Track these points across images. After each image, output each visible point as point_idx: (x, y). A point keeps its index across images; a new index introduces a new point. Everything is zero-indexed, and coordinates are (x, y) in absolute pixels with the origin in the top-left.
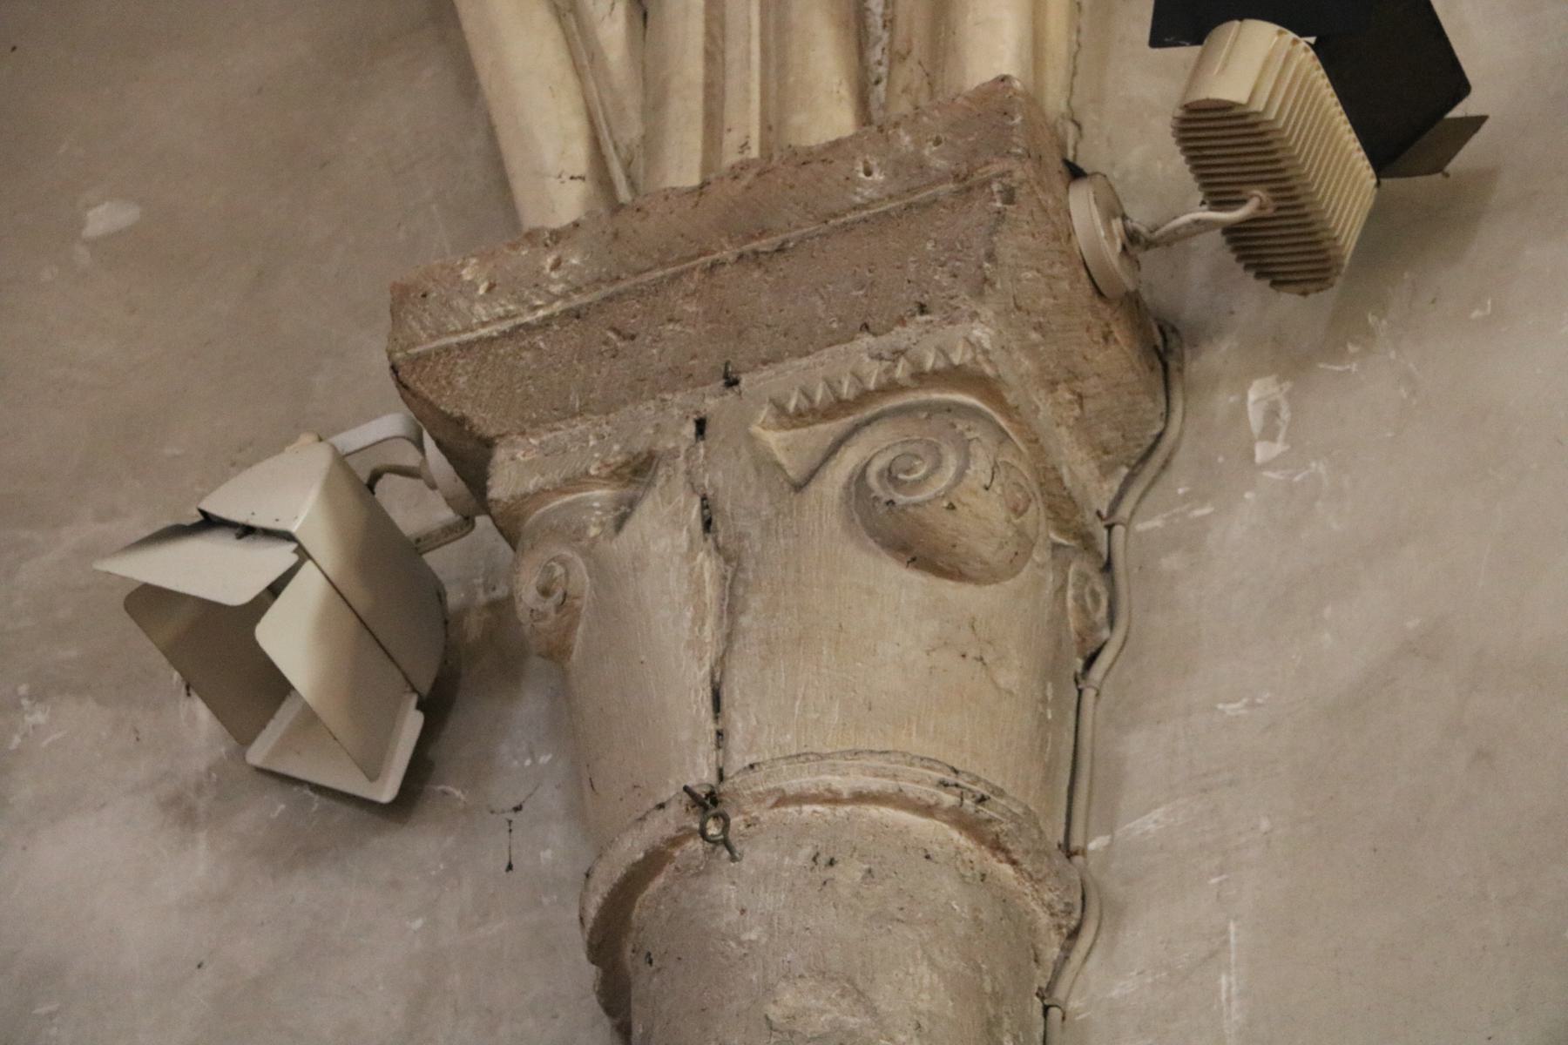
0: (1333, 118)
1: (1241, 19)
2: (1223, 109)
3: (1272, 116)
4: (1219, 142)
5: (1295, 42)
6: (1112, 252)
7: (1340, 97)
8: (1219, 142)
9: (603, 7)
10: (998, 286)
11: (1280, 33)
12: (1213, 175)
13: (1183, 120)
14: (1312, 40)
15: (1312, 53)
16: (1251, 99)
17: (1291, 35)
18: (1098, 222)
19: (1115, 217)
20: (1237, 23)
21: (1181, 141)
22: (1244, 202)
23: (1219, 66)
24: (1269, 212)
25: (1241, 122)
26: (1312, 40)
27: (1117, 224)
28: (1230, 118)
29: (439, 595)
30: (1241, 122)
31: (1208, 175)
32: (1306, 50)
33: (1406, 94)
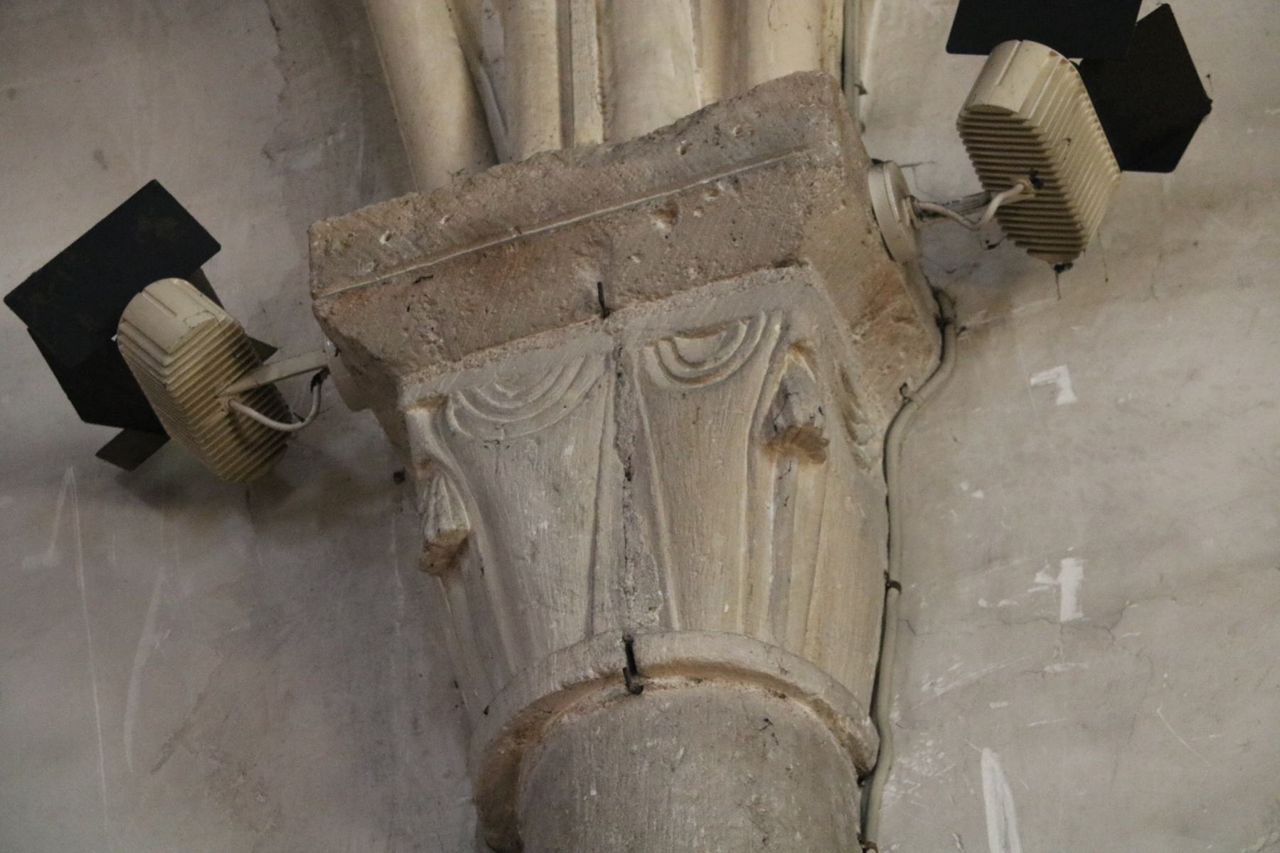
0: (1102, 154)
1: (1021, 40)
2: (1002, 115)
3: (1039, 124)
4: (993, 137)
5: (1063, 62)
6: (903, 230)
7: (1099, 116)
8: (993, 137)
9: (488, 3)
10: (891, 322)
11: (1052, 54)
12: (987, 164)
13: (967, 120)
14: (1078, 61)
15: (1076, 72)
16: (1021, 110)
17: (1061, 57)
18: (893, 200)
19: (905, 198)
20: (1017, 43)
21: (962, 135)
22: (1010, 187)
23: (998, 80)
24: (1031, 196)
25: (1016, 126)
26: (1078, 61)
27: (906, 205)
28: (1006, 122)
29: (751, 557)
30: (1016, 126)
31: (979, 156)
32: (1071, 70)
33: (1153, 106)
